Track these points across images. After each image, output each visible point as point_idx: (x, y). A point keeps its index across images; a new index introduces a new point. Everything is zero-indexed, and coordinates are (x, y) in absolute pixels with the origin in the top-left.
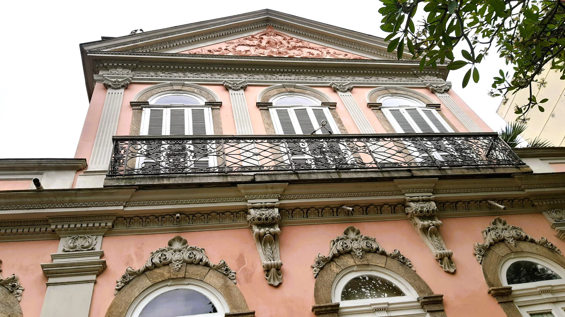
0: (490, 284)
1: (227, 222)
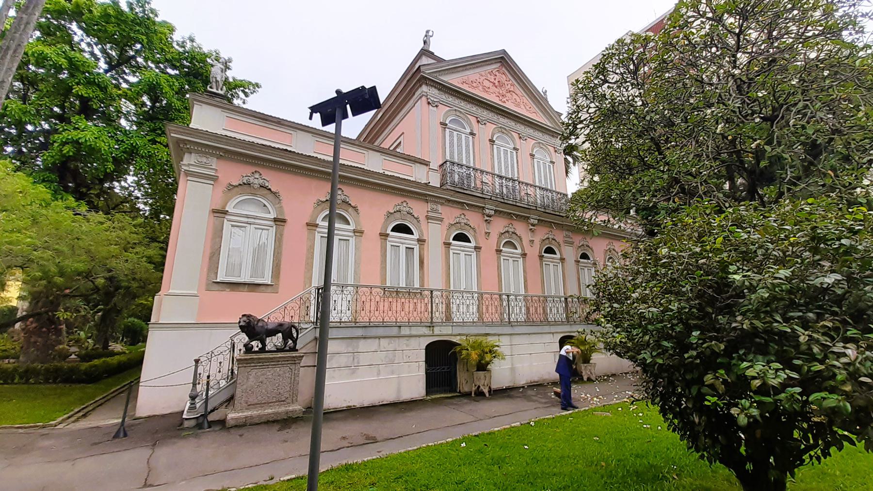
1: (477, 210)
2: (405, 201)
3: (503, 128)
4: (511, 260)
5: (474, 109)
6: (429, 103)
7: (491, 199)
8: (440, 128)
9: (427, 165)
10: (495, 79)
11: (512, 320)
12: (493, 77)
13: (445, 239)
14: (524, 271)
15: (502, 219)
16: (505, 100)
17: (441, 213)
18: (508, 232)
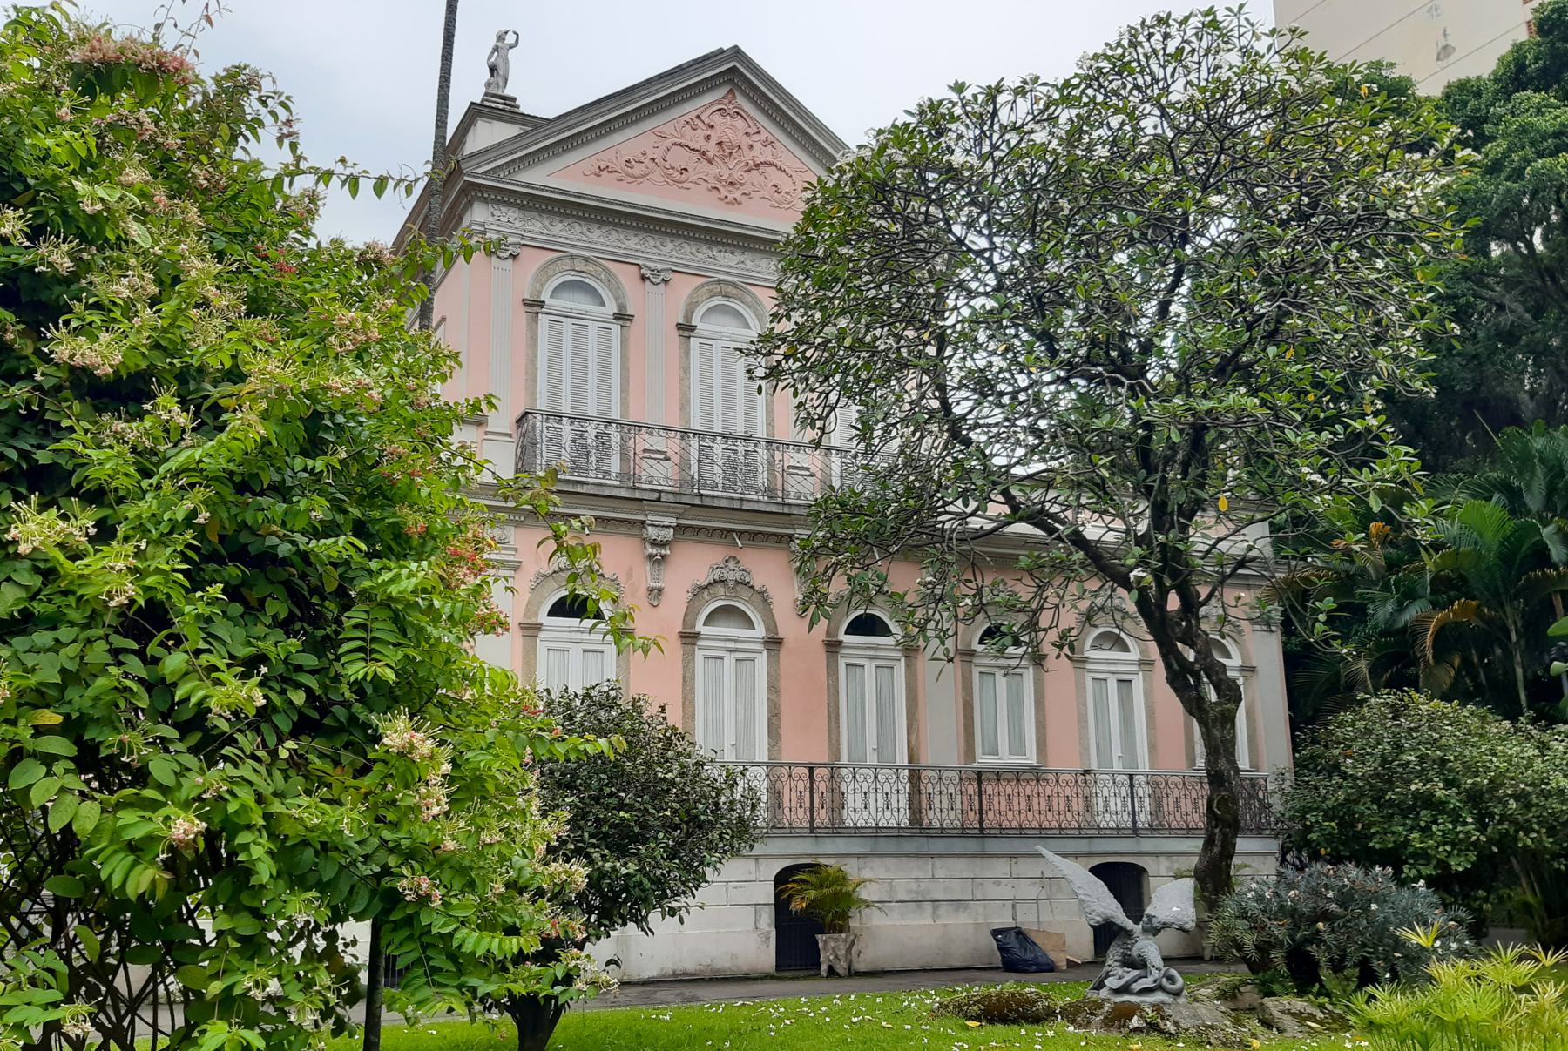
0: (828, 634)
1: (623, 530)
2: (734, 558)
3: (727, 283)
4: (730, 660)
6: (643, 278)
8: (522, 314)
9: (479, 424)
10: (708, 138)
11: (818, 823)
12: (702, 132)
13: (525, 615)
14: (773, 688)
15: (700, 547)
16: (737, 194)
18: (722, 581)
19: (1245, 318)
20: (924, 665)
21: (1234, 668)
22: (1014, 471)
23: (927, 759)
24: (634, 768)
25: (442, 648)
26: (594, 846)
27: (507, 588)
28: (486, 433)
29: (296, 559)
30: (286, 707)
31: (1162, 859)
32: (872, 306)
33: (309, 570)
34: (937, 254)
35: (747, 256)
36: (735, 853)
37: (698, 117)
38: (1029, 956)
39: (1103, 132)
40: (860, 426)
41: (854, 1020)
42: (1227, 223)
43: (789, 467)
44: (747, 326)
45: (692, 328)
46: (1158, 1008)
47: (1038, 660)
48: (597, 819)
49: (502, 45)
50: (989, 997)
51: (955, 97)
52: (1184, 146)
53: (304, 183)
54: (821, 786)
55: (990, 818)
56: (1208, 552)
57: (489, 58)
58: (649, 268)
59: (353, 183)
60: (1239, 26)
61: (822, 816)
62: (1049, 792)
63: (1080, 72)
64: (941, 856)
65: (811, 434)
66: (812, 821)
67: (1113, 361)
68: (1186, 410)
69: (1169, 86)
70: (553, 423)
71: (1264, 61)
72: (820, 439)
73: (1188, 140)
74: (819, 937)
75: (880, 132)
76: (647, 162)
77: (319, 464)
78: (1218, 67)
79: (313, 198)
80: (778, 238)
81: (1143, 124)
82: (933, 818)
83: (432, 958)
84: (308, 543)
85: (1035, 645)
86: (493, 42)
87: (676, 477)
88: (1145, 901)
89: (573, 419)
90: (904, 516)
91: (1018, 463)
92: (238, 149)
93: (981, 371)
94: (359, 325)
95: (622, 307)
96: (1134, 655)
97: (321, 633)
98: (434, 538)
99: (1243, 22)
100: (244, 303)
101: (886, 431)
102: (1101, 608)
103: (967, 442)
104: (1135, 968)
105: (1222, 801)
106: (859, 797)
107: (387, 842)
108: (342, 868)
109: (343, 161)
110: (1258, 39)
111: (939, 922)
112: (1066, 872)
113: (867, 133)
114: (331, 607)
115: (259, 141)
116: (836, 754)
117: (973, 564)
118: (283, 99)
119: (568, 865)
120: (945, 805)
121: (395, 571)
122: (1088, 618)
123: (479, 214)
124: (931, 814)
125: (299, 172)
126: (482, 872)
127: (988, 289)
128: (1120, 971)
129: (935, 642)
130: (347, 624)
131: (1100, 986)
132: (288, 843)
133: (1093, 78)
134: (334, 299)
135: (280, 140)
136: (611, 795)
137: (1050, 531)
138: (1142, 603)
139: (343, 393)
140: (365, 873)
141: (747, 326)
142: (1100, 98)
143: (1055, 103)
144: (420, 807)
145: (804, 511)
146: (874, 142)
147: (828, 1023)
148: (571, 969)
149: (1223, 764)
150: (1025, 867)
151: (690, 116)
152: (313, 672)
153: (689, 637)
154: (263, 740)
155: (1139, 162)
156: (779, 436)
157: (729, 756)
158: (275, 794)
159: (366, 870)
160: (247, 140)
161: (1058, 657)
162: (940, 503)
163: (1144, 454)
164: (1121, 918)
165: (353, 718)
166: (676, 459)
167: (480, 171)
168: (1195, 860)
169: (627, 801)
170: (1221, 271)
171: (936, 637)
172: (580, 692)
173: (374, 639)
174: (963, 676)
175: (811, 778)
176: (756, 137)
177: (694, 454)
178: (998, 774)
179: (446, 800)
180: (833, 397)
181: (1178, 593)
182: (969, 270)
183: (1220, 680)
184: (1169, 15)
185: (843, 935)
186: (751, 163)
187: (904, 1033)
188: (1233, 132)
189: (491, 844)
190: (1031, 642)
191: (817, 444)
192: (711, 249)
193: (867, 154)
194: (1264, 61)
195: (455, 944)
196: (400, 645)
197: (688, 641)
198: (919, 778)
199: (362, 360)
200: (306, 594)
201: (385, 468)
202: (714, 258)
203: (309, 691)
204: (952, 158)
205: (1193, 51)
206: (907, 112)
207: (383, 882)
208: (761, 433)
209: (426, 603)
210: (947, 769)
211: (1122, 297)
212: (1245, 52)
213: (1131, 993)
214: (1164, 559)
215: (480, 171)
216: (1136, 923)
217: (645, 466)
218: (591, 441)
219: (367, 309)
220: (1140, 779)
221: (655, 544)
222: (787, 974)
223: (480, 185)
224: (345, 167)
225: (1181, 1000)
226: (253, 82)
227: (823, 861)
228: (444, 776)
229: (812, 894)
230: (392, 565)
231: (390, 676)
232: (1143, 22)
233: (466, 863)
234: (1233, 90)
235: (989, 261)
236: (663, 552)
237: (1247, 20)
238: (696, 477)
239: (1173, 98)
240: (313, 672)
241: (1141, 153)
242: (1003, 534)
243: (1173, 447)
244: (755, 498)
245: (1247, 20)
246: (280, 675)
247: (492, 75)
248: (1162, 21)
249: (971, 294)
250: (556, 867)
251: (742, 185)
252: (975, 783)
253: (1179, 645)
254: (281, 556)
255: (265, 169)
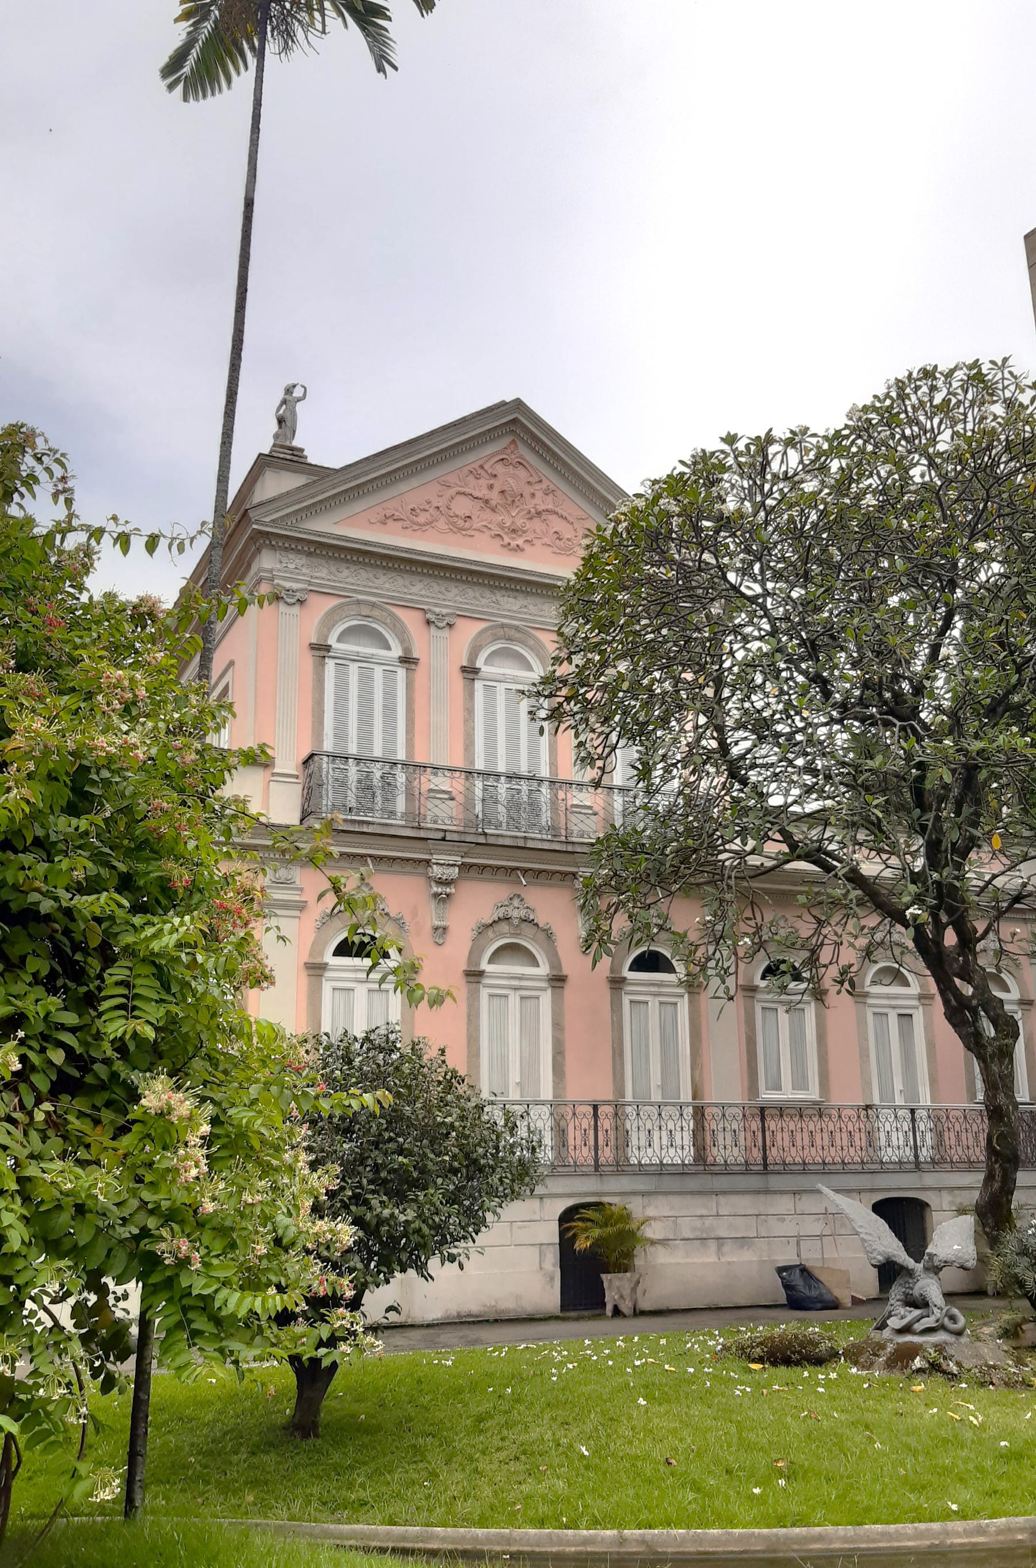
0: (612, 970)
2: (519, 896)
5: (323, 573)
6: (429, 622)
7: (444, 839)
8: (308, 660)
9: (266, 766)
13: (311, 955)
14: (558, 1025)
16: (520, 542)
17: (301, 890)
19: (1014, 661)
20: (708, 1005)
21: (1011, 1002)
22: (791, 809)
23: (712, 1096)
24: (414, 1112)
25: (208, 1001)
26: (373, 1192)
27: (279, 937)
28: (273, 774)
29: (59, 916)
30: (45, 1066)
31: (944, 1193)
32: (651, 648)
33: (72, 926)
34: (713, 600)
35: (529, 601)
36: (515, 1195)
37: (482, 467)
38: (814, 1293)
39: (874, 482)
40: (640, 767)
41: (638, 1363)
42: (996, 567)
43: (573, 806)
44: (530, 668)
45: (476, 671)
46: (940, 1348)
47: (819, 995)
48: (376, 1164)
49: (290, 399)
50: (772, 1338)
51: (726, 447)
52: (953, 494)
53: (73, 541)
54: (606, 1123)
55: (773, 1154)
56: (986, 886)
57: (278, 410)
58: (434, 613)
59: (124, 541)
60: (1003, 379)
61: (607, 1154)
62: (831, 1127)
63: (851, 423)
64: (724, 1193)
65: (591, 774)
66: (596, 1160)
67: (885, 703)
68: (958, 751)
69: (935, 437)
70: (339, 763)
71: (1028, 412)
72: (600, 779)
73: (957, 488)
74: (604, 1276)
75: (655, 482)
76: (431, 510)
77: (83, 824)
78: (983, 418)
79: (88, 553)
80: (559, 583)
81: (912, 473)
82: (717, 1154)
83: (193, 1321)
84: (71, 899)
85: (815, 980)
86: (280, 395)
87: (461, 816)
88: (929, 1239)
89: (358, 760)
90: (684, 855)
91: (795, 802)
92: (13, 505)
93: (758, 711)
94: (126, 683)
95: (407, 650)
96: (914, 989)
97: (83, 989)
98: (200, 891)
99: (1007, 375)
100: (13, 658)
101: (667, 770)
102: (882, 943)
103: (744, 782)
104: (917, 1307)
105: (1002, 1137)
106: (643, 1135)
107: (146, 1203)
108: (99, 1230)
109: (115, 518)
110: (1022, 391)
111: (723, 1260)
112: (847, 1210)
113: (642, 483)
114: (94, 964)
115: (34, 497)
116: (620, 1091)
117: (752, 903)
118: (58, 456)
119: (333, 1224)
120: (729, 1141)
121: (158, 926)
122: (868, 953)
123: (267, 561)
124: (715, 1150)
125: (71, 529)
126: (244, 1233)
127: (763, 633)
128: (902, 1311)
129: (715, 982)
130: (109, 980)
131: (882, 1326)
132: (42, 1209)
133: (862, 428)
134: (101, 658)
135: (55, 496)
136: (390, 1140)
137: (828, 869)
138: (920, 939)
139: (107, 753)
140: (123, 1236)
141: (530, 668)
142: (870, 448)
143: (827, 454)
144: (177, 1170)
145: (586, 849)
146: (650, 491)
147: (611, 1367)
148: (336, 1330)
149: (1001, 1099)
150: (807, 1203)
151: (473, 466)
152: (73, 1030)
153: (474, 975)
154: (20, 1100)
155: (909, 509)
156: (562, 776)
157: (514, 1095)
158: (32, 1156)
159: (124, 1232)
160: (22, 496)
161: (839, 992)
162: (720, 842)
163: (918, 793)
164: (902, 1257)
165: (114, 1076)
166: (460, 799)
167: (267, 519)
168: (976, 1195)
169: (406, 1146)
170: (990, 615)
171: (717, 975)
172: (360, 1035)
173: (137, 996)
174: (746, 1011)
175: (596, 1116)
176: (537, 487)
177: (478, 792)
178: (782, 1110)
179: (205, 1161)
180: (614, 737)
181: (956, 929)
182: (743, 615)
183: (998, 1015)
184: (936, 367)
185: (628, 1274)
186: (533, 510)
187: (686, 1376)
188: (998, 480)
189: (252, 1204)
190: (812, 978)
191: (597, 784)
192: (494, 594)
193: (641, 504)
194: (1028, 412)
195: (217, 1305)
196: (162, 1001)
197: (472, 979)
198: (703, 1115)
199: (130, 713)
200: (68, 950)
201: (152, 823)
202: (497, 602)
203: (68, 1049)
204: (723, 507)
205: (959, 402)
206: (682, 462)
207: (142, 1245)
208: (544, 772)
209: (190, 958)
210: (730, 1105)
211: (893, 640)
212: (1009, 404)
213: (914, 1333)
214: (939, 897)
215: (267, 519)
216: (917, 1261)
217: (430, 805)
218: (376, 781)
219: (136, 665)
220: (921, 1113)
221: (440, 882)
222: (573, 1314)
223: (268, 533)
224: (117, 525)
225: (964, 1340)
226: (30, 437)
227: (606, 1200)
228: (202, 1138)
229: (596, 1232)
230: (156, 920)
231: (150, 1033)
232: (910, 374)
233: (228, 1223)
234: (999, 440)
235: (763, 607)
236: (448, 890)
237: (1011, 373)
238: (480, 816)
239: (941, 447)
240: (73, 1030)
241: (909, 502)
242: (785, 871)
243: (946, 787)
244: (539, 836)
245: (1011, 373)
246: (41, 1034)
247: (280, 427)
248: (928, 374)
249: (746, 640)
250: (322, 1225)
251: (524, 532)
252: (758, 1119)
253: (957, 981)
254: (43, 912)
255: (37, 526)
